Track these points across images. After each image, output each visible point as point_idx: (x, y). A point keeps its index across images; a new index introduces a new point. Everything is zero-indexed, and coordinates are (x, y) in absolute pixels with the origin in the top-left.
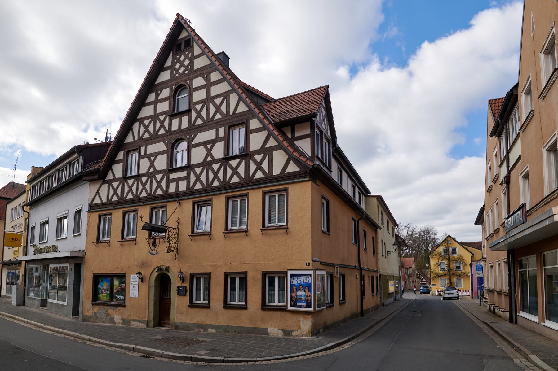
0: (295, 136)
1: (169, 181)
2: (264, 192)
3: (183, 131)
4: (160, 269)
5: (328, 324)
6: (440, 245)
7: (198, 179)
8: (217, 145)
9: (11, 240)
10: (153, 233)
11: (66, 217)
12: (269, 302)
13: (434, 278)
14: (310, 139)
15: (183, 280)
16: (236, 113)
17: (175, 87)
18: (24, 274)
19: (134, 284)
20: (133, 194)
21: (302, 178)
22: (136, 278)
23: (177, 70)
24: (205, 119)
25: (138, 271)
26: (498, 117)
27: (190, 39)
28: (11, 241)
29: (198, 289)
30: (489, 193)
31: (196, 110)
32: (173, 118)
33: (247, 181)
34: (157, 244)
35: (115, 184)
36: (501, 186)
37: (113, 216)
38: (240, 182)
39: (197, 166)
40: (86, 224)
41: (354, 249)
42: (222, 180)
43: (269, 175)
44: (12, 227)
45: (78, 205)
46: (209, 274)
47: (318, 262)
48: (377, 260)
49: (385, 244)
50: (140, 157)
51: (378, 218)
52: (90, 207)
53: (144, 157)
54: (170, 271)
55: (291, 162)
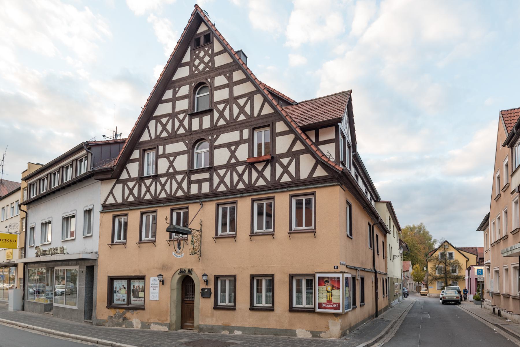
0: (320, 140)
1: (190, 183)
2: (217, 205)
3: (204, 131)
4: (182, 271)
5: (352, 325)
6: (437, 250)
7: (222, 181)
8: (241, 146)
9: (5, 241)
10: (174, 234)
11: (73, 217)
12: (297, 304)
13: (432, 281)
14: (334, 143)
15: (207, 282)
16: (261, 115)
17: (194, 84)
18: (22, 277)
19: (154, 287)
20: (151, 194)
21: (330, 183)
22: (156, 281)
23: (197, 67)
24: (228, 120)
25: (159, 274)
26: (514, 128)
27: (210, 34)
28: (5, 242)
29: (223, 291)
30: (496, 201)
31: (218, 110)
32: (193, 117)
33: (273, 185)
34: (182, 246)
35: (131, 184)
36: (512, 195)
37: (129, 217)
38: (266, 185)
39: (220, 168)
40: (99, 225)
41: (371, 252)
42: (247, 182)
43: (296, 179)
44: (6, 227)
45: (89, 205)
46: (235, 276)
47: (345, 265)
48: (386, 263)
49: (392, 248)
50: (158, 156)
51: (387, 223)
52: (103, 207)
53: (162, 156)
54: (193, 273)
55: (319, 167)
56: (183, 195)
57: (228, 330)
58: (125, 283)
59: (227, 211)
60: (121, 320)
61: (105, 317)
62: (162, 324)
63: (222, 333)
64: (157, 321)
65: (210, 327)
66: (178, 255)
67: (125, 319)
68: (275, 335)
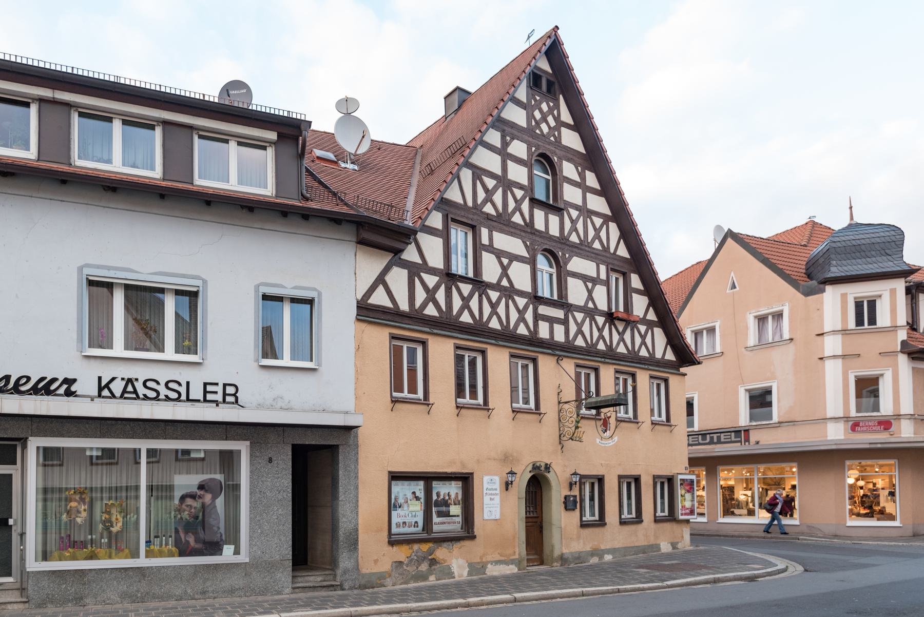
1: (537, 317)
4: (535, 467)
25: (510, 470)
40: (353, 350)
54: (551, 469)
56: (527, 335)
57: (597, 555)
58: (419, 487)
60: (424, 567)
61: (385, 566)
62: (506, 563)
63: (591, 561)
64: (498, 558)
65: (577, 555)
67: (433, 562)
68: (643, 553)
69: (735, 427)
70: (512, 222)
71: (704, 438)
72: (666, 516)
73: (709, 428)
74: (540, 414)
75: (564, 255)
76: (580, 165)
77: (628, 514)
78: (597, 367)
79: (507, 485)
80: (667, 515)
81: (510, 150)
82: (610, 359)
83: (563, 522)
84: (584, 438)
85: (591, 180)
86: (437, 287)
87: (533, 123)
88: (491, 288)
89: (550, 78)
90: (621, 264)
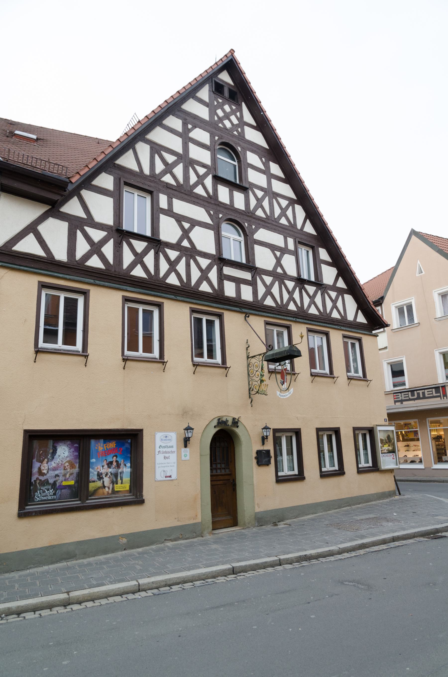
1: (222, 277)
4: (221, 422)
19: (166, 452)
33: (325, 317)
54: (239, 424)
59: (207, 326)
66: (285, 394)
69: (436, 384)
70: (194, 193)
71: (413, 395)
72: (370, 467)
73: (417, 386)
74: (334, 378)
75: (250, 225)
76: (264, 157)
77: (365, 463)
78: (289, 326)
79: (186, 441)
80: (371, 465)
81: (192, 135)
82: (301, 319)
83: (255, 479)
84: (268, 392)
85: (275, 169)
86: (209, 268)
87: (216, 118)
88: (170, 247)
89: (231, 88)
90: (305, 238)
